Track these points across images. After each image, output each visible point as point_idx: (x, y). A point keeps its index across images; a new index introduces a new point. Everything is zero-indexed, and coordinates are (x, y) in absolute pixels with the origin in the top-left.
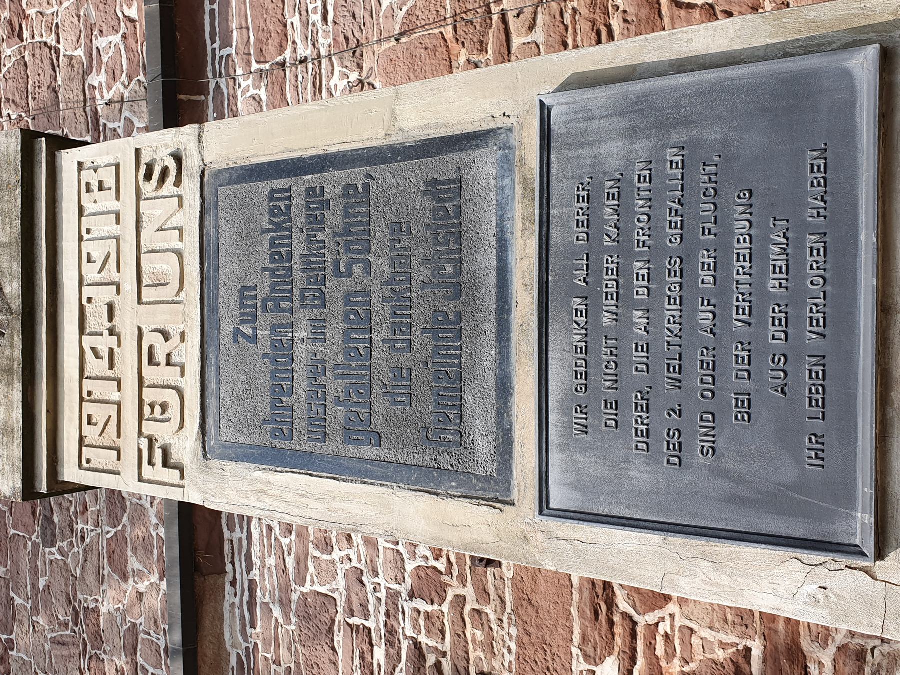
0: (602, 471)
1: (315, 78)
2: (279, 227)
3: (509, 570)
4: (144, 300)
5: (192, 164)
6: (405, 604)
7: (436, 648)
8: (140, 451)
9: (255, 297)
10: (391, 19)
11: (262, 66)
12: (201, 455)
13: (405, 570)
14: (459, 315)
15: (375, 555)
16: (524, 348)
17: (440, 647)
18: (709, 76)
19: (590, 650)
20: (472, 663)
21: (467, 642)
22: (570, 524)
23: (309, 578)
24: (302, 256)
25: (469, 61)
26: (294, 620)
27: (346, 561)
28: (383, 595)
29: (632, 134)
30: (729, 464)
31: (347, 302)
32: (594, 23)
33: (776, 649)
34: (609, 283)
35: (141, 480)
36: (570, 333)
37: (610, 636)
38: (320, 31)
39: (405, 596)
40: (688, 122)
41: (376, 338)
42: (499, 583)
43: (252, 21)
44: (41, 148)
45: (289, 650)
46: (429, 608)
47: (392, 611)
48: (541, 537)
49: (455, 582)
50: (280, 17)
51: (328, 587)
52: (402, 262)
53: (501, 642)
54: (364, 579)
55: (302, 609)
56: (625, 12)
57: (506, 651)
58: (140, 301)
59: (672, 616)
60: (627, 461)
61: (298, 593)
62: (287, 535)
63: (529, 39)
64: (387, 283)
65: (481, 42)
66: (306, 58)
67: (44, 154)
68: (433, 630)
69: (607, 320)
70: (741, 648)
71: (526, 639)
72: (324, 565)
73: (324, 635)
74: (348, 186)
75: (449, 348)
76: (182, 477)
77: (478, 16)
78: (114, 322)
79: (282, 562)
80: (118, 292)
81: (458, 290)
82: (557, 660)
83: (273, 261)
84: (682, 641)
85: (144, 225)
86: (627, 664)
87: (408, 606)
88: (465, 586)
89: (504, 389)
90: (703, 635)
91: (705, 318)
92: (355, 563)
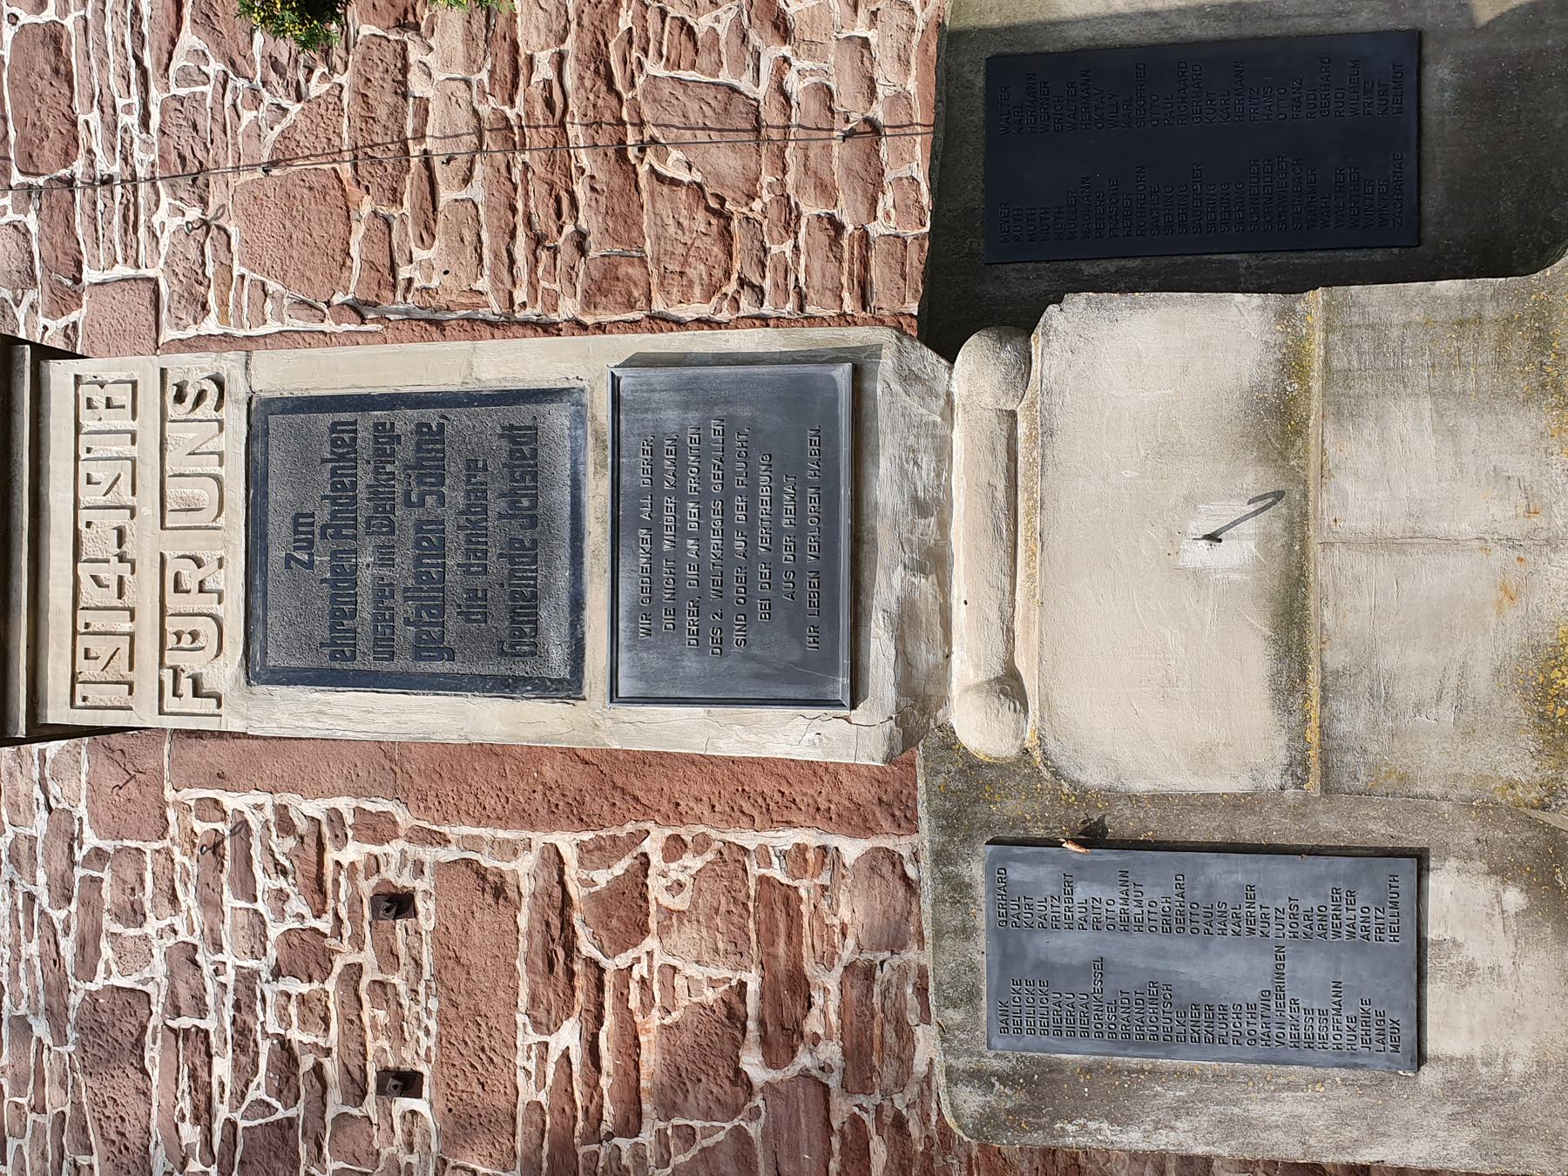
0: (662, 664)
1: (127, 208)
2: (342, 457)
4: (168, 525)
5: (238, 388)
7: (316, 1044)
8: (161, 683)
9: (312, 524)
10: (255, 140)
11: (32, 180)
12: (243, 681)
13: (266, 937)
14: (534, 542)
16: (595, 569)
17: (321, 1042)
18: (741, 370)
19: (541, 1015)
20: (370, 1058)
22: (634, 708)
23: (101, 967)
24: (368, 486)
25: (375, 213)
26: (72, 1035)
27: (168, 932)
28: (229, 978)
29: (686, 406)
30: (755, 651)
32: (552, 185)
33: (775, 977)
34: (668, 519)
35: (161, 712)
36: (637, 557)
37: (569, 992)
38: (136, 140)
39: (265, 975)
40: (727, 402)
41: (450, 562)
42: (413, 939)
43: (14, 108)
44: (23, 356)
45: (63, 1084)
46: (305, 988)
47: (244, 1000)
48: (609, 723)
49: (346, 946)
50: (66, 110)
51: (136, 976)
52: (477, 495)
55: (88, 1016)
56: (592, 177)
57: (421, 1034)
58: (163, 527)
59: (650, 954)
60: (681, 654)
61: (81, 994)
63: (463, 195)
64: (462, 513)
65: (394, 190)
66: (111, 177)
67: (28, 363)
68: (311, 1019)
69: (666, 546)
70: (734, 983)
71: (451, 1013)
72: (129, 945)
73: (127, 1052)
74: (420, 425)
75: (525, 571)
76: (219, 705)
77: (391, 154)
78: (124, 548)
79: (53, 947)
80: (132, 516)
81: (533, 522)
82: (496, 1034)
83: (334, 488)
84: (662, 983)
85: (170, 447)
87: (270, 990)
88: (361, 950)
89: (577, 604)
90: (688, 972)
91: (739, 545)
92: (183, 936)
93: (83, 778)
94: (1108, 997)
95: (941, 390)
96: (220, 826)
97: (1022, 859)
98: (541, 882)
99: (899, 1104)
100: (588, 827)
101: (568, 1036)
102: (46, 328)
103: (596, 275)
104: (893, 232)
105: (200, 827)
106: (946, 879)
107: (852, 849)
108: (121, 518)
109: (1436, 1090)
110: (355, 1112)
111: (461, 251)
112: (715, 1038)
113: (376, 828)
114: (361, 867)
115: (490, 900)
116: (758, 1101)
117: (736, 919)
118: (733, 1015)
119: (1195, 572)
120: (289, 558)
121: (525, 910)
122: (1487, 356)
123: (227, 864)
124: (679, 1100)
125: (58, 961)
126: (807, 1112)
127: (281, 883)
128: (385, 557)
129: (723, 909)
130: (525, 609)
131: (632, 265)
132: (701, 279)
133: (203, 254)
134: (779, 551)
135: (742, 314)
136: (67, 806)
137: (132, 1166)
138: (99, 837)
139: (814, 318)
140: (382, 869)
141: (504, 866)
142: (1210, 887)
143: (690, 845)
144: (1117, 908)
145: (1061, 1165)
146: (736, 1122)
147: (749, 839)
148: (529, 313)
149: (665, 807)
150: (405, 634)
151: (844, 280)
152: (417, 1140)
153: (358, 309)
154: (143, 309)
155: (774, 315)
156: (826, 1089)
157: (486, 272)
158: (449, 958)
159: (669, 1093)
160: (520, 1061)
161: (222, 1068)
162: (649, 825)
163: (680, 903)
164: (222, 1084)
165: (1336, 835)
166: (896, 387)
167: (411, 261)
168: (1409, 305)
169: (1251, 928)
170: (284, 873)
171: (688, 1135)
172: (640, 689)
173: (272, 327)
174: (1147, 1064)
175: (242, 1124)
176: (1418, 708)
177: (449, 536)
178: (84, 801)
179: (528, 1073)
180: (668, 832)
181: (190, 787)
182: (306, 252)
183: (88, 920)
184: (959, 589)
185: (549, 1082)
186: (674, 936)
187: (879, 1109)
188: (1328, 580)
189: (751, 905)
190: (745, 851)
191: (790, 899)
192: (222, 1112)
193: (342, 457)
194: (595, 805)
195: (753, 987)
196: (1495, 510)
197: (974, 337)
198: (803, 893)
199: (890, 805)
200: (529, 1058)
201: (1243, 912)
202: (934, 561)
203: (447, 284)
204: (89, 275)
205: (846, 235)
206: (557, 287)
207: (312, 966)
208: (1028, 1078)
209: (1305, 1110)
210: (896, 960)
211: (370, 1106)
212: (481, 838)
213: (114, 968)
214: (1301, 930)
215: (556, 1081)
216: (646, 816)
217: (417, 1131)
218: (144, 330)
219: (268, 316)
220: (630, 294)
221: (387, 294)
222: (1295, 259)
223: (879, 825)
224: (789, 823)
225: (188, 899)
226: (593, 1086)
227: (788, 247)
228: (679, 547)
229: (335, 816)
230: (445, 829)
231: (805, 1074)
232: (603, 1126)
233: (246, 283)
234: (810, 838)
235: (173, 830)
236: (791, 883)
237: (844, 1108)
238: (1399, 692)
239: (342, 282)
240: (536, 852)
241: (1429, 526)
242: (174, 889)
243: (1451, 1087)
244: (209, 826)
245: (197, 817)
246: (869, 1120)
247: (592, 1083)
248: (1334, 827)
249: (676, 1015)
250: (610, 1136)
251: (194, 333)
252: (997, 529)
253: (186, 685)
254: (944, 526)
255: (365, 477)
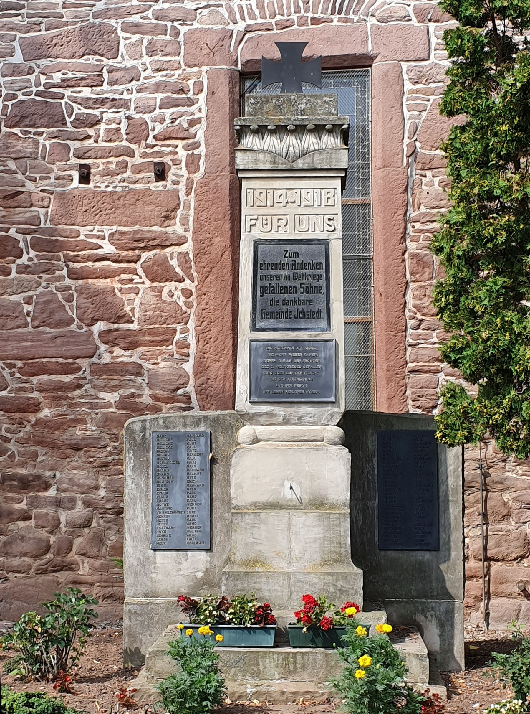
2: (313, 265)
3: (155, 187)
5: (332, 236)
6: (122, 113)
7: (99, 136)
13: (144, 113)
14: (291, 318)
15: (151, 91)
17: (100, 139)
19: (117, 236)
20: (95, 161)
21: (107, 158)
23: (128, 35)
28: (126, 96)
29: (325, 359)
30: (263, 377)
31: (294, 287)
33: (135, 336)
34: (296, 354)
37: (127, 248)
39: (128, 113)
40: (326, 369)
41: (286, 295)
42: (145, 180)
46: (123, 131)
49: (142, 150)
53: (111, 181)
54: (134, 82)
57: (106, 184)
59: (143, 283)
61: (115, 25)
62: (155, 16)
69: (290, 354)
70: (133, 319)
71: (115, 197)
79: (136, 12)
82: (107, 217)
84: (132, 288)
86: (113, 258)
88: (141, 157)
89: (275, 330)
90: (137, 300)
91: (290, 373)
92: (143, 74)
93: (210, 26)
94: (169, 465)
95: (329, 423)
96: (191, 92)
97: (206, 442)
98: (172, 236)
99: (87, 387)
100: (195, 257)
101: (108, 248)
102: (409, 6)
103: (425, 259)
104: (440, 383)
105: (191, 83)
106: (200, 420)
107: (188, 367)
108: (298, 202)
109: (146, 555)
110: (71, 154)
111: (437, 200)
112: (110, 311)
113: (192, 164)
114: (176, 157)
115: (164, 214)
116: (85, 329)
117: (159, 319)
118: (121, 318)
119: (283, 484)
120: (287, 251)
121: (160, 229)
122: (333, 549)
123: (175, 96)
124: (84, 296)
125: (130, 14)
126: (83, 349)
127: (168, 121)
128: (287, 278)
129: (163, 314)
130: (273, 315)
131: (429, 274)
132: (423, 304)
133: (439, 82)
134: (287, 382)
135: (408, 321)
136: (198, 18)
137: (42, 50)
138: (185, 34)
139: (406, 351)
140: (175, 167)
141: (178, 220)
142: (200, 493)
143: (188, 300)
144: (194, 468)
145: (66, 451)
146: (76, 319)
147: (191, 325)
148: (410, 229)
149: (204, 289)
150: (267, 283)
151: (421, 363)
152: (61, 182)
153: (413, 153)
154: (416, 54)
155: (407, 334)
156: (91, 357)
157: (428, 211)
158: (140, 196)
159: (87, 292)
160: (97, 227)
161: (86, 92)
162: (196, 283)
163: (165, 296)
164: (79, 92)
165: (216, 527)
166: (330, 412)
167: (433, 177)
168: (345, 532)
169: (189, 505)
170: (172, 122)
171: (69, 299)
172: (253, 347)
173: (407, 114)
174: (150, 476)
175: (63, 102)
176: (252, 534)
177: (293, 295)
178: (200, 26)
179: (91, 231)
180: (193, 291)
181: (208, 79)
182: (439, 130)
183: (148, 29)
184: (279, 428)
185: (89, 240)
186: (152, 293)
187: (84, 378)
188: (281, 513)
189: (164, 326)
190: (186, 323)
191: (168, 342)
192: (68, 92)
193: (313, 265)
194: (204, 260)
195: (131, 326)
196: (297, 551)
197: (342, 431)
198: (170, 347)
199: (207, 383)
200: (98, 231)
201: (194, 502)
202: (286, 422)
203: (423, 193)
204: (432, 26)
205: (439, 364)
206: (421, 241)
207: (133, 135)
208: (144, 443)
209: (139, 519)
210: (144, 385)
211: (74, 161)
212: (189, 210)
213: (128, 42)
214: (189, 518)
215: (90, 243)
216: (200, 281)
217: (64, 181)
218: (406, 55)
219: (411, 113)
220: (417, 273)
221: (420, 166)
222: (376, 516)
223: (199, 378)
224: (198, 341)
225: (159, 77)
226: (88, 259)
227: (435, 340)
228: (289, 357)
229: (197, 145)
230: (193, 194)
231: (97, 348)
232: (72, 263)
233: (426, 103)
234: (193, 350)
235: (189, 70)
236: (174, 342)
237: (84, 364)
238: (255, 529)
239: (425, 146)
240: (184, 234)
241: (293, 536)
242: (163, 70)
243: (148, 558)
244: (191, 87)
245: (195, 82)
246: (80, 374)
247: (89, 258)
248: (218, 527)
249: (119, 294)
250: (68, 266)
251: (405, 78)
252: (294, 437)
253: (253, 222)
254: (295, 424)
255: (308, 272)
